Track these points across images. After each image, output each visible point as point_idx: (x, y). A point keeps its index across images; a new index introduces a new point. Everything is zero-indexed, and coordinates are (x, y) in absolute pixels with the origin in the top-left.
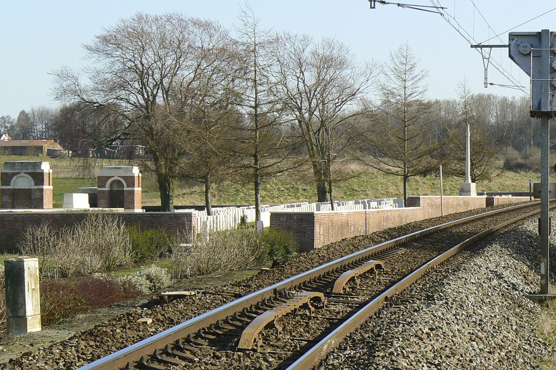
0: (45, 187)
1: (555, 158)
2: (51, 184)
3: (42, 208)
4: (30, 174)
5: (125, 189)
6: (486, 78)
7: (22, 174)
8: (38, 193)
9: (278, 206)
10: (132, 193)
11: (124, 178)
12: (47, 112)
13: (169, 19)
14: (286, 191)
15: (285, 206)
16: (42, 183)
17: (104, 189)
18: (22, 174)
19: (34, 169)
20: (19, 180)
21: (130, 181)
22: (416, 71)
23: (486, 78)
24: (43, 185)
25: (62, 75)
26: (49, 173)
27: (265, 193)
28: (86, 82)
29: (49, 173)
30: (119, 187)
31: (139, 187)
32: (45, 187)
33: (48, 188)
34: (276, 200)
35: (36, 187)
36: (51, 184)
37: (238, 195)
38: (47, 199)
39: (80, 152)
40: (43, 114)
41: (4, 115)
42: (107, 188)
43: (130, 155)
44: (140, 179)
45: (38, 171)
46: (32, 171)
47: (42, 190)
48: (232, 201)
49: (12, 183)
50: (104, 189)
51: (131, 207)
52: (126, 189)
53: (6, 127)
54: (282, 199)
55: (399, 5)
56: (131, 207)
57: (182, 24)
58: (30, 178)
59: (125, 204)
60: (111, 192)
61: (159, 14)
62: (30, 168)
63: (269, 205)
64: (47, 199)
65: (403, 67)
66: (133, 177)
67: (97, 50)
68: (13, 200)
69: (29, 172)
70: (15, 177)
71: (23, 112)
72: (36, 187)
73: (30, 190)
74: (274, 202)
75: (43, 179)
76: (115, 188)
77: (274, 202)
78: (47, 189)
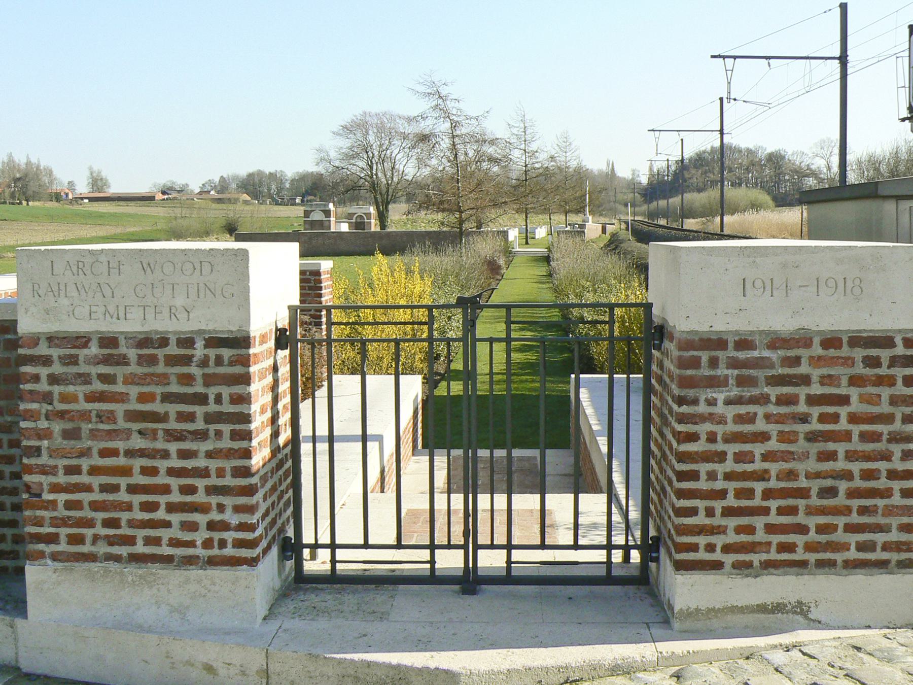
4: (321, 210)
6: (657, 150)
8: (328, 223)
12: (237, 176)
13: (385, 114)
17: (308, 219)
20: (316, 214)
21: (369, 215)
22: (572, 146)
23: (657, 150)
25: (319, 150)
28: (333, 154)
33: (333, 219)
35: (326, 219)
39: (261, 202)
40: (235, 178)
41: (111, 181)
42: (354, 221)
43: (367, 202)
45: (327, 209)
47: (330, 221)
50: (308, 219)
52: (366, 221)
53: (211, 186)
55: (744, 101)
57: (392, 118)
60: (356, 222)
61: (378, 112)
65: (565, 144)
66: (370, 213)
67: (340, 135)
70: (312, 213)
71: (222, 177)
72: (326, 219)
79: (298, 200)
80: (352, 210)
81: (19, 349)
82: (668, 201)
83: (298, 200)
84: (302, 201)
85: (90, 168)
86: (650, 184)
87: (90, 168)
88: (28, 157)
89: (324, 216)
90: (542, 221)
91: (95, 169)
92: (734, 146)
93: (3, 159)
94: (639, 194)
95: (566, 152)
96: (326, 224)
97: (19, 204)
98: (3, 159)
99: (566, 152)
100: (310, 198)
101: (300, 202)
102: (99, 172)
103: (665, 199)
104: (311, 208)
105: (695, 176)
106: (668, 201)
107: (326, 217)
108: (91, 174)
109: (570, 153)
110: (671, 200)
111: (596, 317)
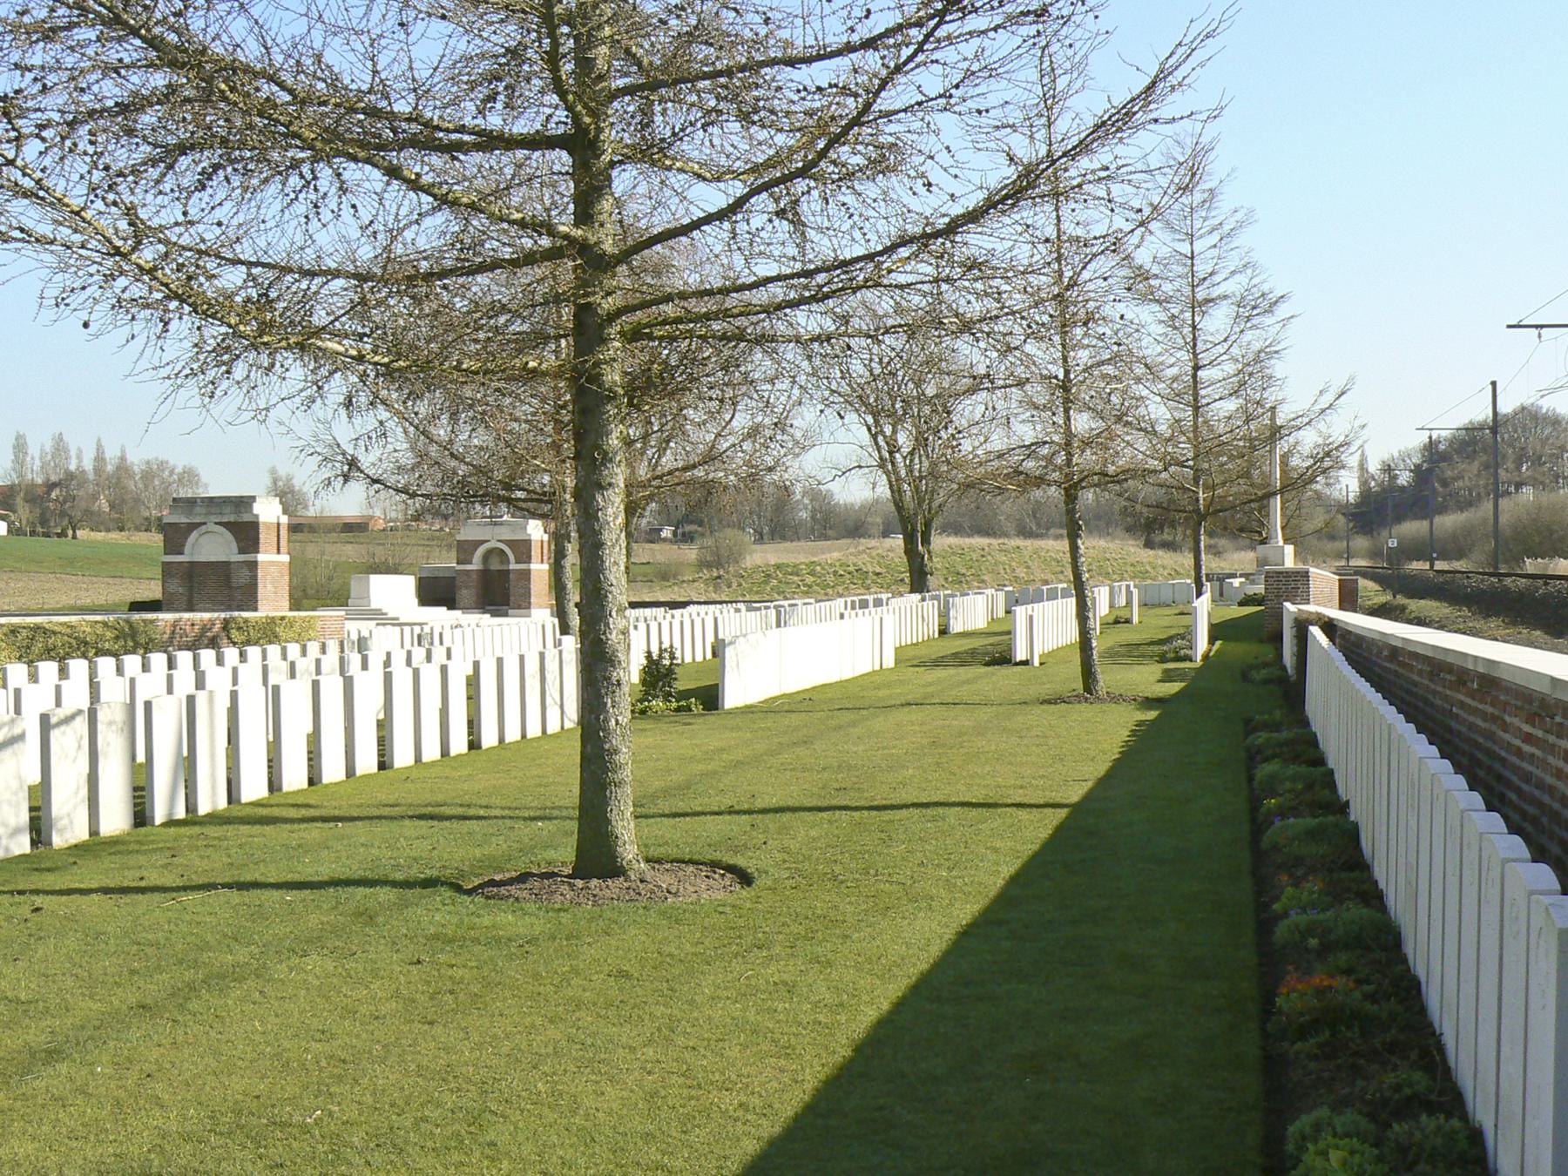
0: (261, 557)
1: (565, 2)
2: (284, 548)
3: (256, 609)
4: (226, 525)
5: (511, 567)
7: (211, 527)
8: (245, 572)
9: (827, 603)
10: (526, 574)
11: (511, 543)
14: (848, 576)
15: (853, 602)
16: (528, 560)
17: (468, 567)
18: (211, 527)
19: (238, 512)
21: (523, 549)
22: (1224, 205)
24: (258, 552)
26: (278, 524)
27: (812, 579)
29: (278, 524)
30: (502, 562)
31: (279, 552)
32: (261, 557)
34: (830, 591)
35: (242, 558)
36: (284, 548)
37: (766, 583)
38: (269, 587)
42: (476, 565)
44: (284, 533)
45: (246, 518)
46: (232, 519)
47: (253, 565)
48: (757, 592)
49: (187, 549)
50: (468, 567)
51: (524, 604)
52: (513, 566)
54: (840, 589)
56: (524, 604)
58: (228, 536)
59: (512, 598)
62: (228, 510)
63: (812, 601)
64: (269, 587)
68: (191, 589)
69: (225, 520)
70: (195, 534)
72: (242, 558)
73: (227, 564)
74: (826, 594)
75: (258, 539)
76: (495, 565)
77: (826, 594)
78: (272, 563)
79: (667, 533)
80: (468, 533)
81: (1292, 547)
82: (1431, 523)
83: (667, 533)
84: (675, 533)
85: (273, 471)
86: (1365, 494)
87: (273, 471)
88: (123, 451)
89: (234, 546)
90: (1130, 569)
91: (282, 472)
92: (1544, 411)
93: (43, 446)
94: (1343, 514)
95: (1191, 237)
96: (241, 578)
97: (59, 535)
98: (43, 446)
99: (1191, 237)
100: (689, 528)
101: (670, 535)
102: (289, 479)
103: (1423, 518)
104: (190, 513)
105: (1468, 474)
106: (1431, 523)
107: (242, 551)
108: (275, 481)
109: (1215, 238)
110: (1438, 520)
111: (924, 31)
